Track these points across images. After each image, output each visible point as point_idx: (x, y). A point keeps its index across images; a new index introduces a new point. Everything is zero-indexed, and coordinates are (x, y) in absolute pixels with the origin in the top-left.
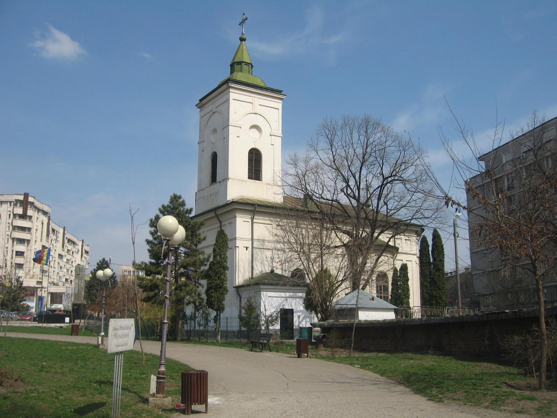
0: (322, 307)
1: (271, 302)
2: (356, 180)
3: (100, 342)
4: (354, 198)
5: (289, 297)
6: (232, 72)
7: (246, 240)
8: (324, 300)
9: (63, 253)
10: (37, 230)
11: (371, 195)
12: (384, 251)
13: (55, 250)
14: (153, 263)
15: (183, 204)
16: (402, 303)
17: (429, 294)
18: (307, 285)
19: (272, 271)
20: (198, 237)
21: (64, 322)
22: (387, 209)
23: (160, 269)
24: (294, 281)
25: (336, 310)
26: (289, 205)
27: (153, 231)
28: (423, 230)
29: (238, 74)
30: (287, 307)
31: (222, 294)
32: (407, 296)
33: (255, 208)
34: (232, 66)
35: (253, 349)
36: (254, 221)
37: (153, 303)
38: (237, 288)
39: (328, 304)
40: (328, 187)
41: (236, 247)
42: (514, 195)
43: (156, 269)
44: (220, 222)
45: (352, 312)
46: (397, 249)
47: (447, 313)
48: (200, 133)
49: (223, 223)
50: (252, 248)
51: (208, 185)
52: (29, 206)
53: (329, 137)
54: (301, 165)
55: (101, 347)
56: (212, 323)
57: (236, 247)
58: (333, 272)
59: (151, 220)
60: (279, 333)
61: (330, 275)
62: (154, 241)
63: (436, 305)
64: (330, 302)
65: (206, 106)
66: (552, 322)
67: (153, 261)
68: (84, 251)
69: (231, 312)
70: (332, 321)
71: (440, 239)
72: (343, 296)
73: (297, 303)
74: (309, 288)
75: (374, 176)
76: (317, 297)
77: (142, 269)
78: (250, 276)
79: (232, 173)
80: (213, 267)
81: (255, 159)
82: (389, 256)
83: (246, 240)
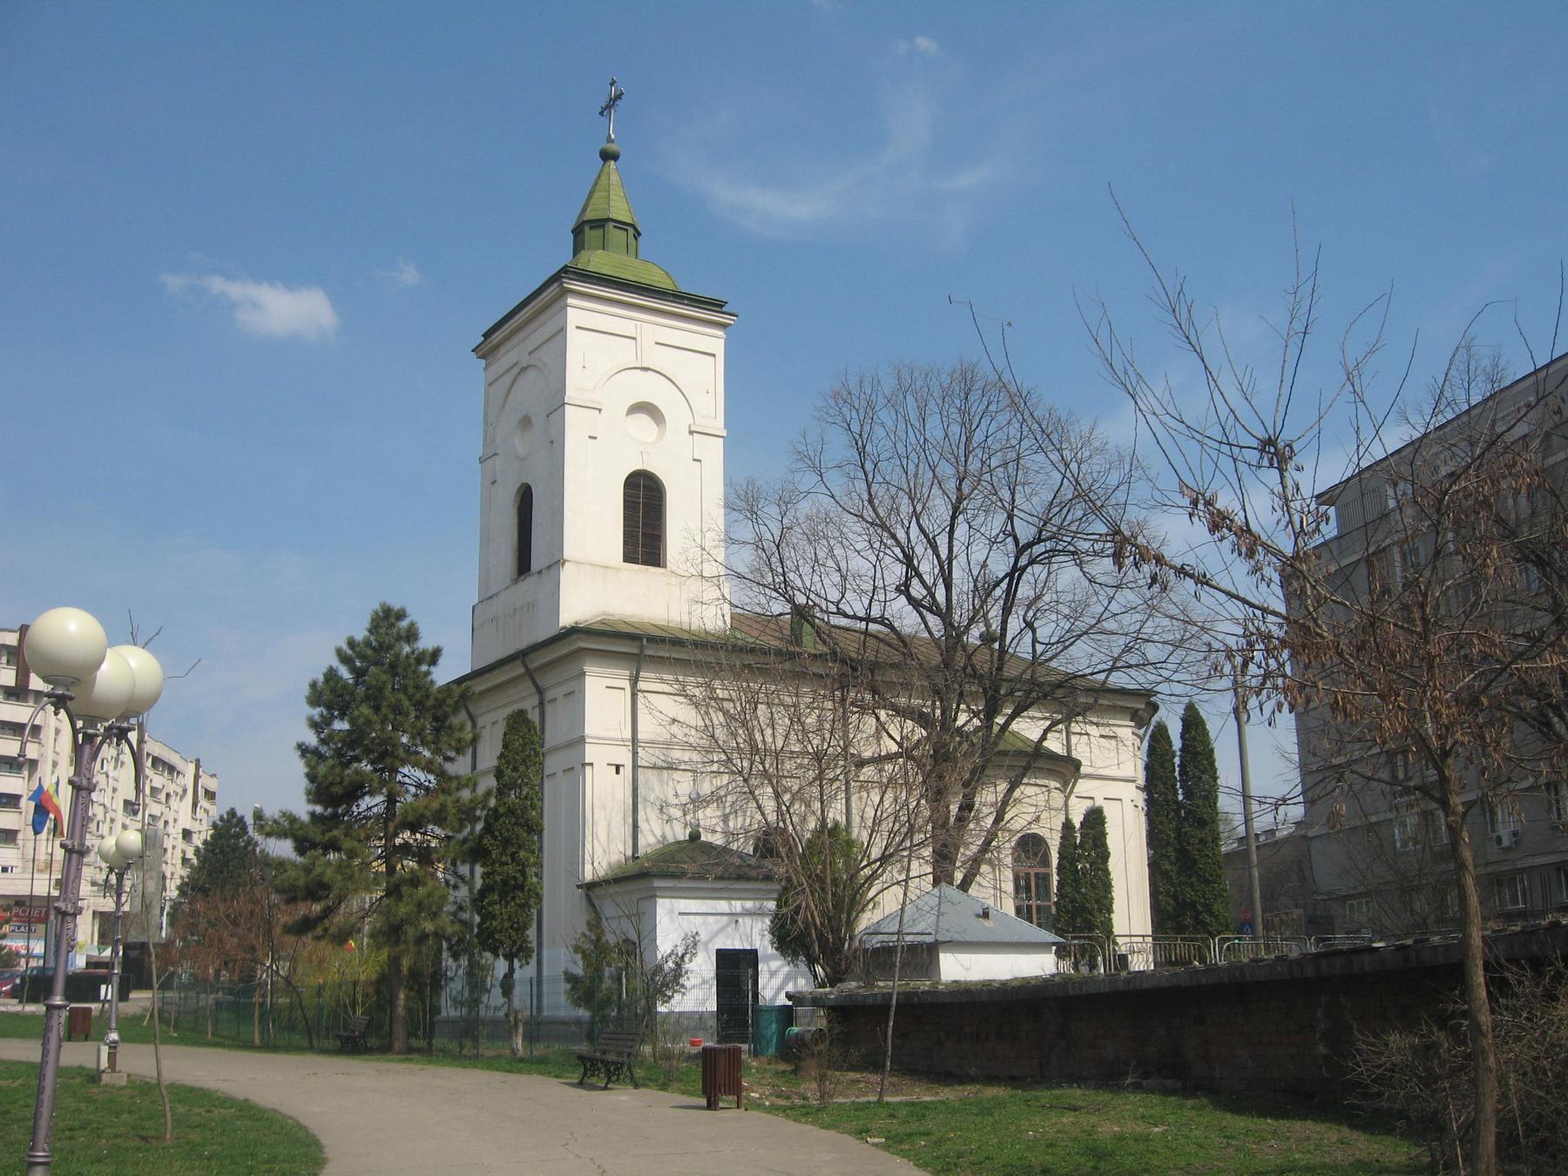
2: (938, 557)
3: (104, 1063)
4: (934, 609)
6: (576, 251)
12: (1025, 771)
13: (115, 790)
14: (322, 815)
15: (411, 635)
16: (1090, 927)
17: (1175, 898)
19: (695, 836)
20: (457, 735)
21: (96, 999)
22: (1035, 641)
23: (335, 833)
26: (747, 637)
27: (317, 718)
28: (1155, 708)
29: (596, 254)
31: (525, 906)
32: (1106, 906)
33: (642, 648)
34: (578, 232)
35: (586, 1080)
36: (642, 685)
37: (318, 938)
38: (590, 887)
40: (856, 581)
41: (584, 765)
43: (323, 833)
44: (540, 692)
46: (1077, 764)
47: (1216, 955)
48: (485, 433)
49: (549, 695)
50: (635, 766)
51: (508, 582)
53: (855, 428)
55: (106, 1078)
56: (496, 998)
57: (584, 765)
58: (860, 834)
59: (313, 685)
60: (712, 1023)
61: (850, 843)
62: (323, 749)
65: (503, 350)
66: (1520, 983)
67: (319, 809)
68: (201, 792)
70: (854, 984)
71: (1205, 733)
72: (886, 907)
75: (993, 542)
77: (283, 834)
78: (629, 853)
79: (572, 547)
80: (497, 826)
81: (644, 502)
82: (1053, 784)
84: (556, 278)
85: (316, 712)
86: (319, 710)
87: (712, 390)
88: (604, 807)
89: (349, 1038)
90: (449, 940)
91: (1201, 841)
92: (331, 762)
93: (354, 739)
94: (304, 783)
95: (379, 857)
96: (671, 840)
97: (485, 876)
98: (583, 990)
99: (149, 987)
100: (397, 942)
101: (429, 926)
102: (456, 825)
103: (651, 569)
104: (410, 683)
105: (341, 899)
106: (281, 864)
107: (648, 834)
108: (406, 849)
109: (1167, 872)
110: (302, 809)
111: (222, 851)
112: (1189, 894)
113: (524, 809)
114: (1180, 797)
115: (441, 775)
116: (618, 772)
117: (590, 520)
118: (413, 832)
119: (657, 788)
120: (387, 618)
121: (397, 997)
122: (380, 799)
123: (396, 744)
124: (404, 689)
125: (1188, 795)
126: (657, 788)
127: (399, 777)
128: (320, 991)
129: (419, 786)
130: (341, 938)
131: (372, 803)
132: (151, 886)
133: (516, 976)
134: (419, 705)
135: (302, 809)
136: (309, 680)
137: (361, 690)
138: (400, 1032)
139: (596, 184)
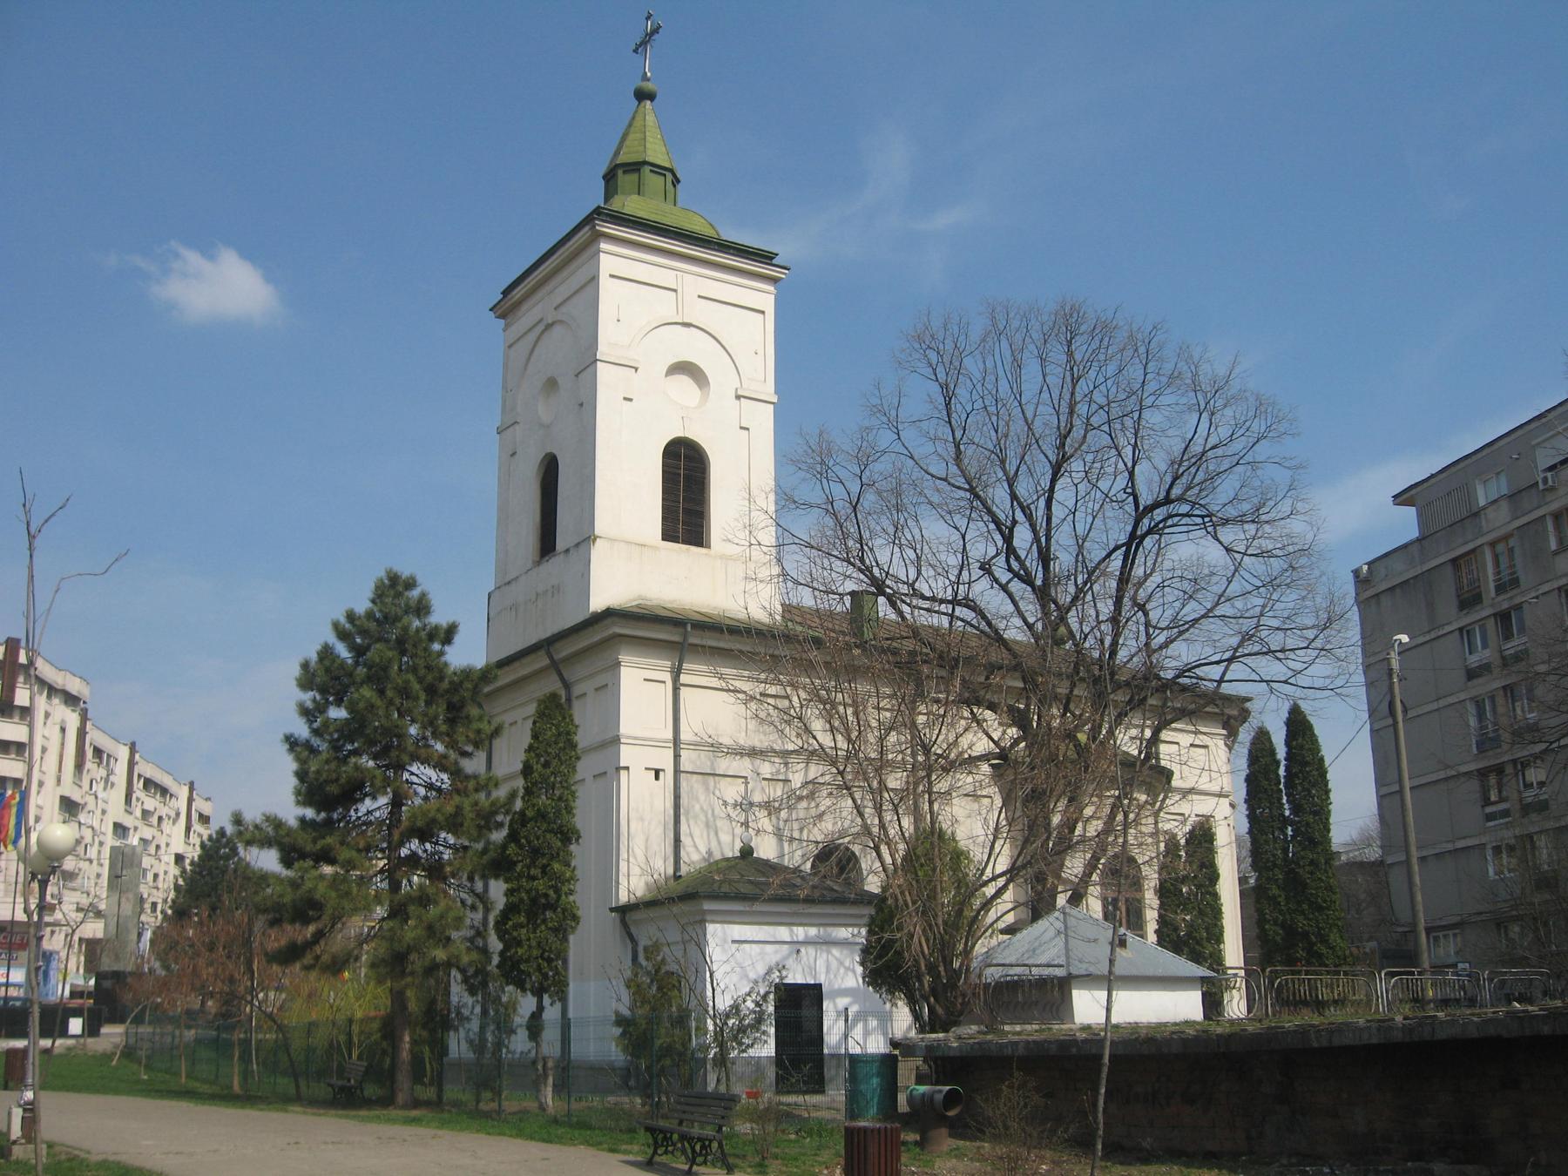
0: (936, 977)
1: (739, 961)
3: (16, 1131)
5: (806, 943)
6: (608, 196)
7: (655, 744)
8: (944, 949)
9: (128, 821)
10: (44, 750)
11: (1090, 574)
13: (104, 812)
14: (313, 821)
15: (422, 608)
17: (1283, 926)
18: (866, 899)
19: (747, 852)
20: (475, 726)
21: (64, 1033)
23: (329, 840)
24: (823, 886)
25: (987, 986)
27: (309, 704)
29: (626, 198)
30: (796, 977)
31: (562, 932)
33: (685, 636)
34: (610, 177)
36: (684, 678)
37: (307, 968)
38: (623, 911)
39: (956, 965)
40: (939, 561)
41: (618, 769)
42: (1518, 607)
43: (314, 841)
45: (1051, 993)
48: (504, 401)
51: (529, 565)
52: (21, 679)
53: (942, 376)
54: (846, 470)
55: (18, 1152)
56: (520, 1043)
57: (618, 769)
59: (305, 666)
60: (771, 1073)
62: (316, 742)
63: (1309, 963)
64: (967, 952)
65: (525, 307)
67: (310, 813)
68: (195, 816)
69: (596, 994)
70: (974, 1028)
73: (834, 964)
74: (880, 909)
76: (917, 941)
77: (266, 843)
78: (670, 871)
79: (603, 522)
80: (523, 832)
81: (685, 471)
83: (655, 744)
84: (588, 220)
85: (308, 697)
86: (311, 694)
87: (761, 352)
88: (642, 819)
89: (342, 1089)
90: (463, 971)
91: (1312, 862)
92: (325, 756)
93: (354, 729)
94: (293, 781)
95: (382, 871)
96: (718, 856)
97: (509, 893)
98: (635, 1033)
99: (122, 1021)
100: (403, 974)
101: (440, 954)
102: (474, 833)
103: (693, 548)
104: (421, 663)
105: (336, 919)
106: (264, 878)
107: (691, 849)
108: (413, 860)
109: (1275, 897)
110: (291, 812)
111: (210, 873)
112: (1301, 923)
113: (558, 813)
114: (1287, 813)
115: (456, 773)
116: (657, 778)
117: (626, 493)
118: (422, 841)
119: (702, 798)
120: (394, 587)
121: (401, 1039)
122: (383, 800)
123: (402, 736)
124: (414, 670)
125: (1296, 809)
126: (702, 798)
127: (406, 776)
128: (311, 1027)
129: (430, 786)
130: (336, 967)
131: (375, 806)
132: (128, 908)
133: (545, 1016)
134: (431, 691)
135: (291, 812)
136: (301, 659)
137: (361, 671)
138: (403, 1080)
139: (630, 125)
